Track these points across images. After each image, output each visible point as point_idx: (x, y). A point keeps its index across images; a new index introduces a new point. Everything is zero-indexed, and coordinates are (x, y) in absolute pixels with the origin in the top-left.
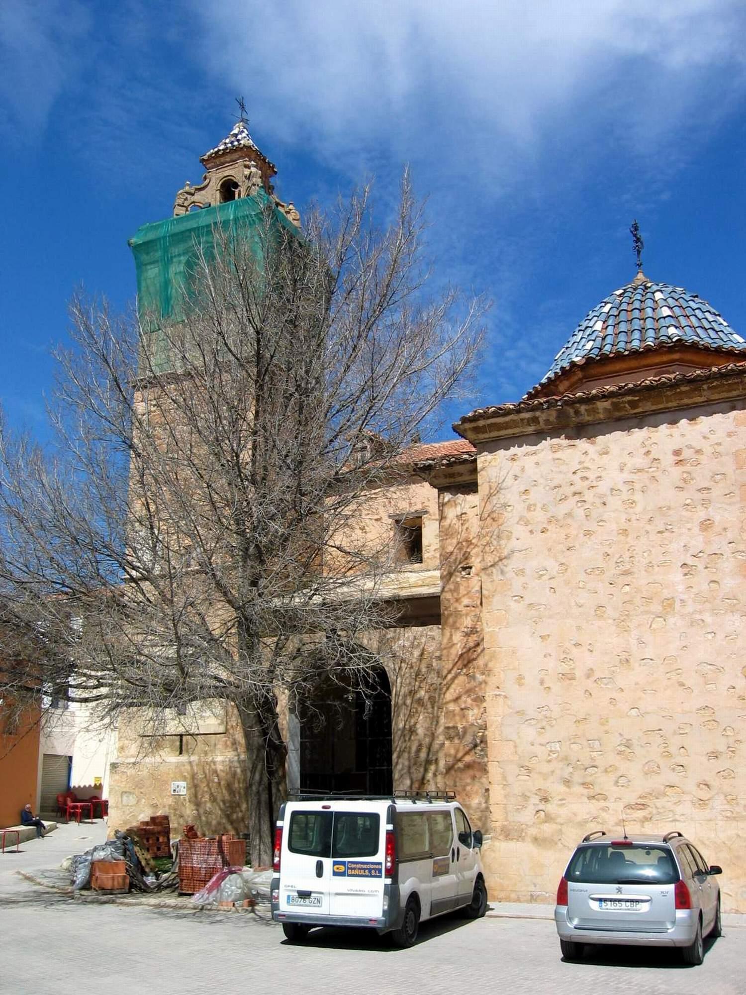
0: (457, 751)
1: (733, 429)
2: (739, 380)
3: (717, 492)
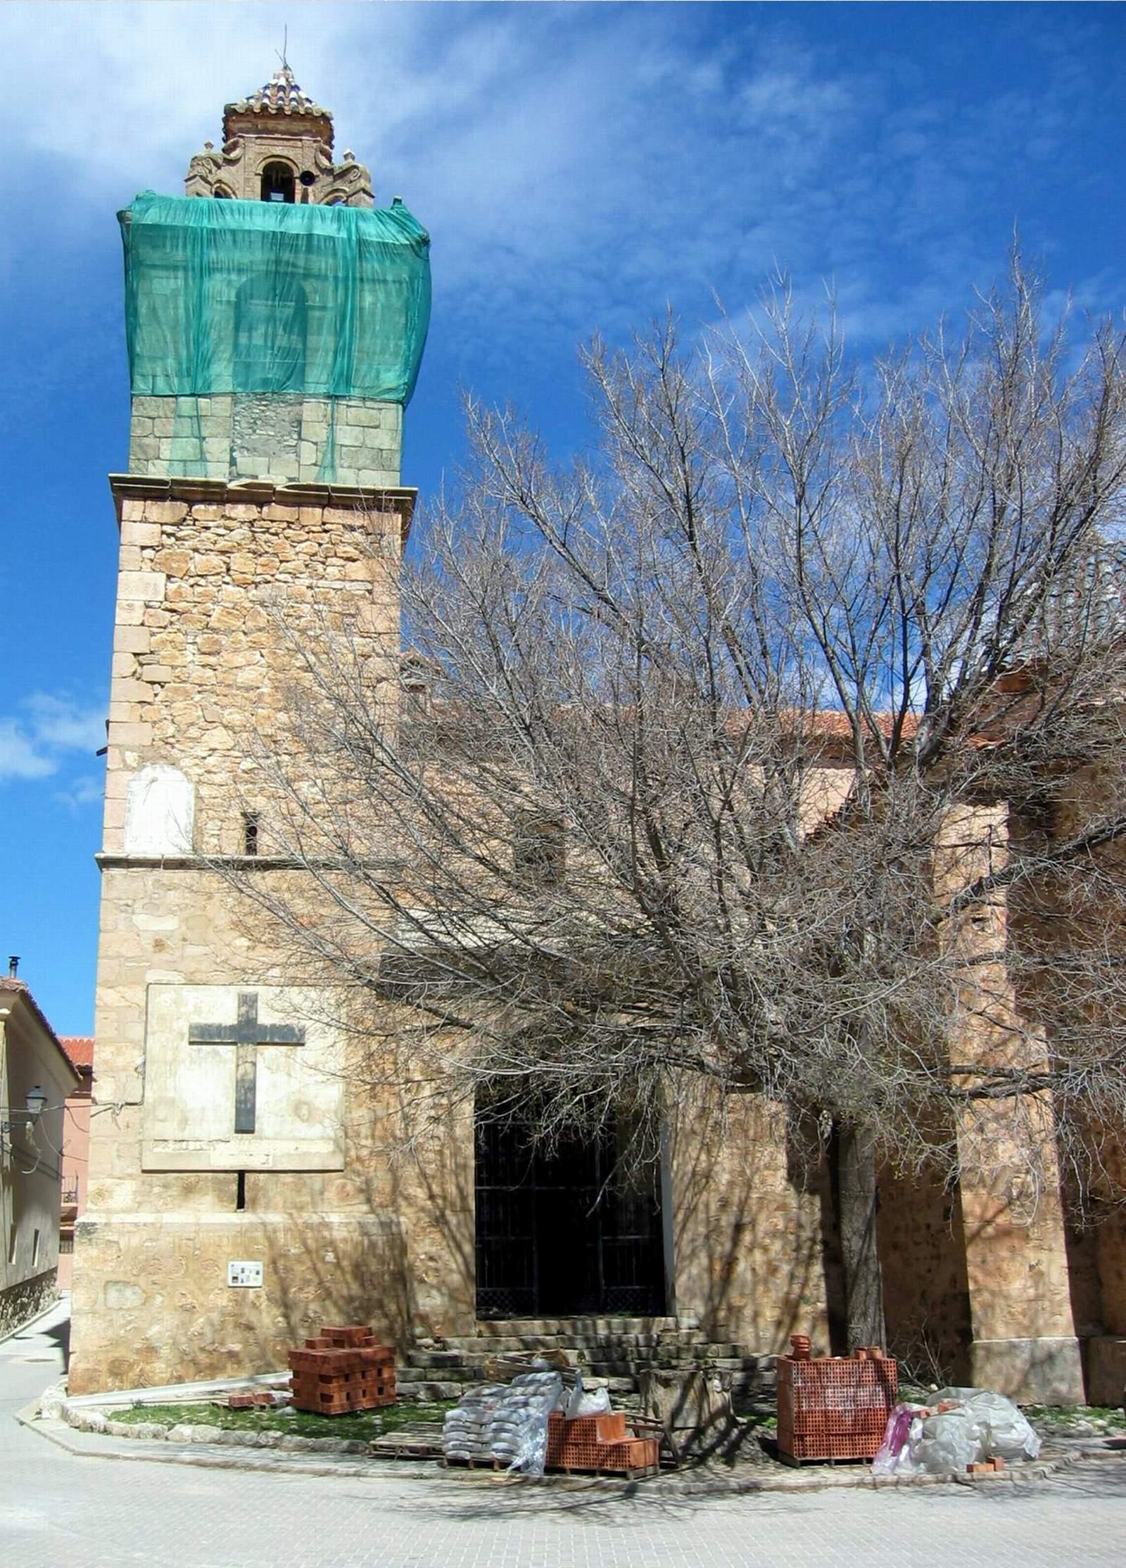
0: (985, 1208)
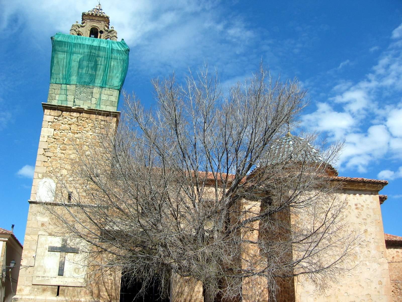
1: (372, 201)
2: (376, 186)
3: (369, 221)
